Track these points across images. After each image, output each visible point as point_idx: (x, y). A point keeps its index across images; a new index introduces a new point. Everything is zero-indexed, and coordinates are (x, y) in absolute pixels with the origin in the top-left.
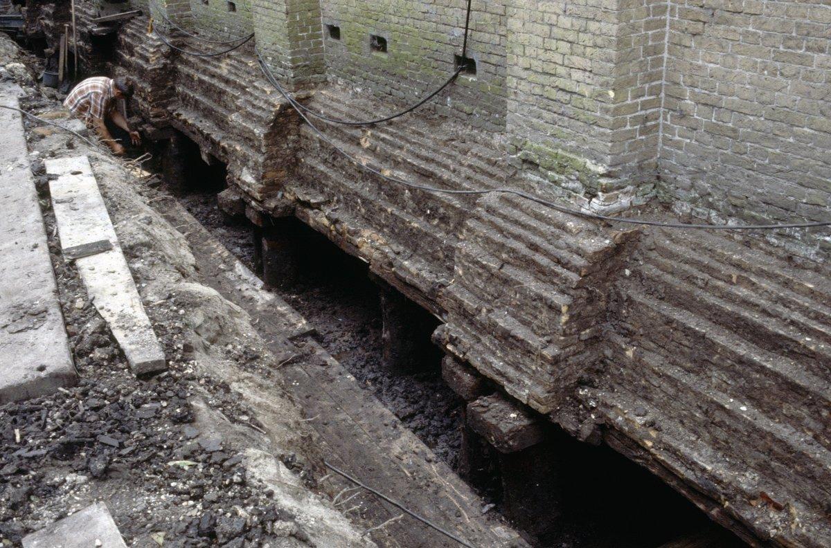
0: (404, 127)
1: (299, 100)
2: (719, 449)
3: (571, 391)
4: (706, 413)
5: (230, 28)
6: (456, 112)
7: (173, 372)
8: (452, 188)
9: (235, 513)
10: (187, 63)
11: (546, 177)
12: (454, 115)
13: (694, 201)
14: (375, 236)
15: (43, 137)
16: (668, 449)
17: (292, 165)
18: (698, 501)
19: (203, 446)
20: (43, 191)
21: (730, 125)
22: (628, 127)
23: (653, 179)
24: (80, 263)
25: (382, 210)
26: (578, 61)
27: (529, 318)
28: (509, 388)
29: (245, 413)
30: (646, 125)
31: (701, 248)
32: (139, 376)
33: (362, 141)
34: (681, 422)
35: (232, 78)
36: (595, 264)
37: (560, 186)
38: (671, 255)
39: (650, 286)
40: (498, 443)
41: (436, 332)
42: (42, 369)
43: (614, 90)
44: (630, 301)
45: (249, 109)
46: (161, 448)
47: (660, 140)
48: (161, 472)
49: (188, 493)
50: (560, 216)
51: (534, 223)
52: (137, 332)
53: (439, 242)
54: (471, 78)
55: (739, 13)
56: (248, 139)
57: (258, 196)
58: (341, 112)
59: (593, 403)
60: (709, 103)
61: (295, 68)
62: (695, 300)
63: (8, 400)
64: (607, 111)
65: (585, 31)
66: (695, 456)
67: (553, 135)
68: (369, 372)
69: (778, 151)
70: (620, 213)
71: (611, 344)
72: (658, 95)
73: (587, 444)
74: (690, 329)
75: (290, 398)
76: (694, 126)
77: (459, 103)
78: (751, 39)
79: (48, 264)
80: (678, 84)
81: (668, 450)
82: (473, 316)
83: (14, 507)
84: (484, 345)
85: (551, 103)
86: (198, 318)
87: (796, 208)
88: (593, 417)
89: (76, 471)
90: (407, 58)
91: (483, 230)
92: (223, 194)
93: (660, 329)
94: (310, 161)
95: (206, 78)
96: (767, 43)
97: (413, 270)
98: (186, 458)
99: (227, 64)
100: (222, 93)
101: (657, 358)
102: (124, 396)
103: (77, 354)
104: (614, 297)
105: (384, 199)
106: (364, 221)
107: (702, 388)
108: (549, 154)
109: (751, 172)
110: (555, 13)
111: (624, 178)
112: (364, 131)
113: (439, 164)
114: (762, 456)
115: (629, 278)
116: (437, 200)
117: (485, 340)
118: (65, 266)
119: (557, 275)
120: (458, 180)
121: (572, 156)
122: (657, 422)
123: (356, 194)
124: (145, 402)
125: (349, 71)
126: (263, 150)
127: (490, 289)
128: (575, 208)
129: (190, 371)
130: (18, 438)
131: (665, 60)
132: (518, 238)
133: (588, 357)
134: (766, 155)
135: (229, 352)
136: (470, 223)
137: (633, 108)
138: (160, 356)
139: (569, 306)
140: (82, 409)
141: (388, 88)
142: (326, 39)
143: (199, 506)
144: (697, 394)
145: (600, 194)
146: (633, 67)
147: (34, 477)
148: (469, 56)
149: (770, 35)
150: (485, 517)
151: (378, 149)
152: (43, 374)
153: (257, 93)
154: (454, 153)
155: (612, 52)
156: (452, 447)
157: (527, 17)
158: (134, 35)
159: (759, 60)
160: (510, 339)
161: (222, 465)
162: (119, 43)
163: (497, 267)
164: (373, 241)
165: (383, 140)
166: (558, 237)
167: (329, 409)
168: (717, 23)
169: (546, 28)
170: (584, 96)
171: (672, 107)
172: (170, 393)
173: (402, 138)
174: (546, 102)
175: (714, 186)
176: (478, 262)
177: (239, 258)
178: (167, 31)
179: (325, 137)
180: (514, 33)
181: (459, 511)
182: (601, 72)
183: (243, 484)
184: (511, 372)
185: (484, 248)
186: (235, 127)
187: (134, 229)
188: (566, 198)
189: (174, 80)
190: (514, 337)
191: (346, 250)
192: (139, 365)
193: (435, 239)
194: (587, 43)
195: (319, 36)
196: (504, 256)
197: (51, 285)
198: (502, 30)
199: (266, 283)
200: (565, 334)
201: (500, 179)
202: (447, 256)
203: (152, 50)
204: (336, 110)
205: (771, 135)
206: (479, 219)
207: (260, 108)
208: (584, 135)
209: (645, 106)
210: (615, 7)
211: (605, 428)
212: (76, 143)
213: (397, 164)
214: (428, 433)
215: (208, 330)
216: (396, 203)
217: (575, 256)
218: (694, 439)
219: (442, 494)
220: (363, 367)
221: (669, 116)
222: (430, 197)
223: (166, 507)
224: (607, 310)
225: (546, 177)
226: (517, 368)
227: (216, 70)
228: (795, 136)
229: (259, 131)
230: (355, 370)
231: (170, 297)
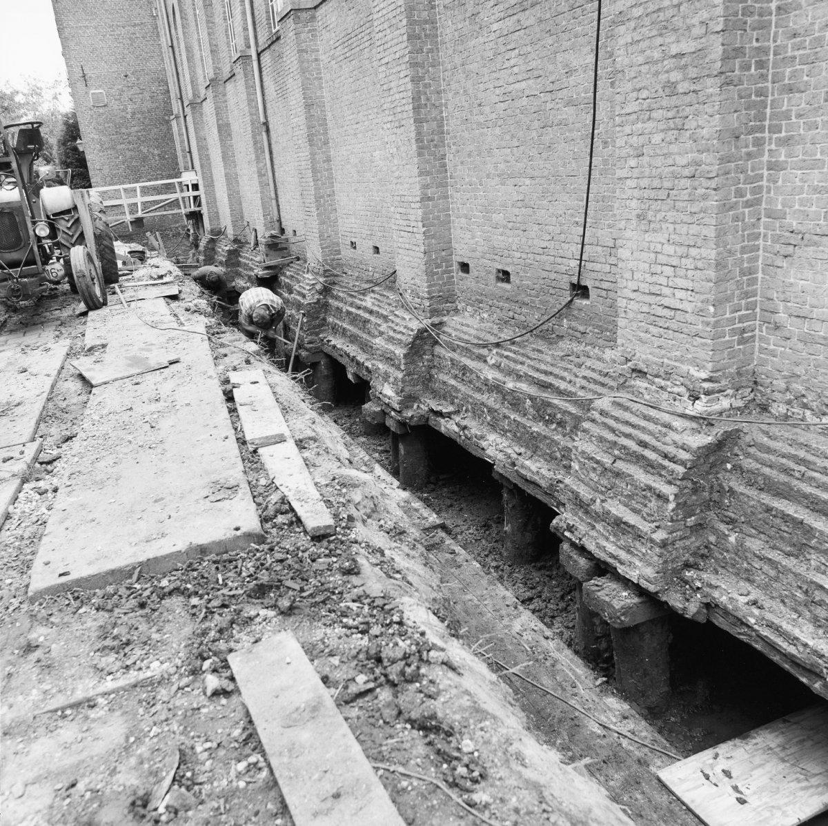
0: (526, 346)
1: (433, 325)
2: (820, 626)
3: (676, 572)
4: (806, 592)
6: (571, 331)
7: (340, 537)
8: (568, 396)
9: (396, 644)
10: (337, 298)
11: (653, 383)
12: (569, 335)
13: (789, 402)
14: (499, 440)
15: (226, 355)
16: (770, 625)
17: (427, 381)
18: (801, 674)
19: (368, 592)
20: (230, 398)
22: (727, 338)
23: (751, 384)
24: (260, 451)
25: (505, 417)
26: (681, 283)
27: (639, 507)
28: (621, 569)
29: (398, 572)
30: (744, 337)
31: (797, 444)
32: (313, 538)
33: (488, 359)
34: (783, 601)
35: (375, 308)
36: (699, 457)
37: (666, 390)
38: (769, 450)
39: (751, 479)
40: (611, 618)
41: (554, 521)
42: (237, 529)
44: (732, 491)
45: (391, 333)
46: (333, 593)
47: (757, 349)
48: (334, 611)
49: (357, 628)
50: (666, 418)
51: (643, 423)
52: (311, 504)
53: (557, 444)
54: (585, 302)
56: (389, 359)
57: (397, 407)
58: (470, 335)
59: (698, 584)
61: (430, 299)
62: (792, 489)
63: (211, 553)
64: (708, 324)
65: (687, 256)
66: (796, 632)
67: (659, 347)
68: (492, 560)
70: (721, 414)
71: (715, 531)
73: (692, 623)
74: (788, 515)
75: (431, 567)
76: (788, 336)
77: (574, 324)
79: (237, 452)
81: (771, 627)
82: (588, 505)
83: (221, 631)
85: (657, 319)
86: (357, 496)
88: (699, 596)
89: (267, 608)
91: (596, 430)
92: (366, 406)
93: (760, 516)
94: (442, 377)
95: (353, 310)
97: (534, 468)
98: (354, 601)
100: (366, 321)
101: (758, 542)
102: (303, 552)
103: (264, 520)
104: (716, 488)
105: (508, 408)
106: (489, 427)
107: (801, 570)
111: (724, 383)
112: (490, 350)
113: (556, 376)
115: (730, 471)
116: (556, 407)
117: (599, 527)
118: (251, 455)
119: (664, 468)
120: (573, 390)
121: (677, 364)
122: (760, 601)
123: (483, 404)
124: (319, 557)
125: (477, 300)
126: (403, 367)
127: (604, 482)
128: (680, 410)
129: (353, 536)
130: (221, 582)
131: (760, 279)
132: (628, 436)
133: (694, 542)
135: (381, 526)
136: (586, 425)
138: (331, 522)
139: (676, 495)
140: (269, 561)
143: (366, 638)
144: (796, 575)
145: (702, 396)
146: (731, 286)
147: (235, 610)
150: (598, 690)
152: (238, 533)
153: (398, 320)
154: (569, 366)
155: (711, 274)
156: (568, 627)
157: (635, 247)
160: (622, 525)
161: (383, 608)
163: (610, 462)
164: (497, 445)
165: (507, 357)
166: (665, 435)
167: (457, 590)
168: (806, 246)
169: (653, 256)
171: (767, 320)
172: (338, 552)
173: (523, 355)
174: (654, 319)
175: (808, 389)
176: (592, 458)
177: (378, 461)
178: (321, 272)
179: (455, 356)
181: (574, 682)
183: (400, 623)
184: (623, 555)
185: (598, 446)
186: (378, 349)
187: (302, 427)
188: (672, 401)
189: (326, 312)
190: (625, 523)
191: (474, 453)
192: (313, 529)
193: (553, 441)
194: (688, 267)
196: (616, 452)
197: (240, 467)
198: (612, 260)
199: (401, 483)
200: (672, 521)
201: (611, 388)
202: (564, 456)
203: (308, 288)
204: (465, 333)
206: (593, 421)
207: (400, 332)
209: (741, 320)
210: (713, 235)
211: (709, 606)
212: (252, 360)
213: (519, 377)
214: (545, 615)
215: (365, 507)
216: (518, 411)
217: (681, 451)
218: (795, 617)
219: (558, 667)
220: (487, 556)
221: (764, 328)
222: (549, 405)
223: (340, 638)
224: (711, 500)
226: (629, 552)
229: (400, 352)
230: (479, 558)
231: (334, 479)
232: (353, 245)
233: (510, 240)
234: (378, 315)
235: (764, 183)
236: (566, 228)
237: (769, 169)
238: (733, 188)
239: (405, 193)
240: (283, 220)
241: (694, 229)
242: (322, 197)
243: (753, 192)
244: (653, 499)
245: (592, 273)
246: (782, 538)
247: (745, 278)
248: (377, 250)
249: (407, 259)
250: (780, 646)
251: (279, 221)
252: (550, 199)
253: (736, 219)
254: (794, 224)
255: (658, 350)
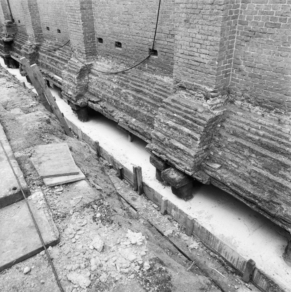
5: (58, 39)
11: (189, 92)
13: (243, 100)
21: (259, 74)
22: (221, 75)
23: (227, 93)
25: (122, 104)
26: (203, 51)
28: (177, 166)
35: (61, 57)
43: (218, 61)
54: (155, 57)
55: (265, 33)
57: (75, 99)
60: (251, 66)
61: (86, 53)
64: (215, 69)
65: (207, 40)
69: (277, 83)
72: (231, 63)
77: (150, 66)
78: (269, 43)
80: (239, 59)
84: (167, 151)
85: (192, 66)
87: (283, 103)
90: (130, 50)
96: (276, 44)
99: (58, 52)
108: (190, 84)
109: (266, 90)
110: (195, 33)
114: (271, 188)
121: (200, 85)
125: (106, 54)
127: (169, 132)
131: (234, 50)
134: (273, 84)
137: (223, 68)
139: (201, 138)
141: (122, 61)
142: (97, 43)
145: (211, 98)
146: (224, 53)
148: (155, 49)
149: (277, 41)
151: (120, 82)
155: (218, 48)
157: (183, 35)
158: (21, 41)
159: (272, 50)
162: (15, 44)
169: (191, 39)
170: (205, 64)
174: (190, 66)
175: (251, 95)
180: (177, 40)
182: (213, 55)
194: (207, 44)
195: (95, 42)
203: (29, 47)
205: (275, 77)
208: (205, 78)
209: (227, 67)
210: (220, 31)
221: (234, 71)
225: (189, 92)
227: (54, 54)
228: (285, 78)
229: (75, 76)
232: (48, 28)
233: (122, 29)
234: (62, 60)
235: (240, 9)
236: (147, 25)
237: (242, 3)
238: (229, 10)
239: (73, 6)
240: (13, 15)
241: (211, 28)
242: (32, 5)
243: (236, 13)
244: (191, 140)
245: (159, 45)
246: (240, 153)
247: (229, 50)
248: (59, 31)
249: (75, 36)
250: (240, 193)
251: (11, 15)
252: (140, 11)
253: (229, 24)
254: (251, 27)
255: (191, 79)
